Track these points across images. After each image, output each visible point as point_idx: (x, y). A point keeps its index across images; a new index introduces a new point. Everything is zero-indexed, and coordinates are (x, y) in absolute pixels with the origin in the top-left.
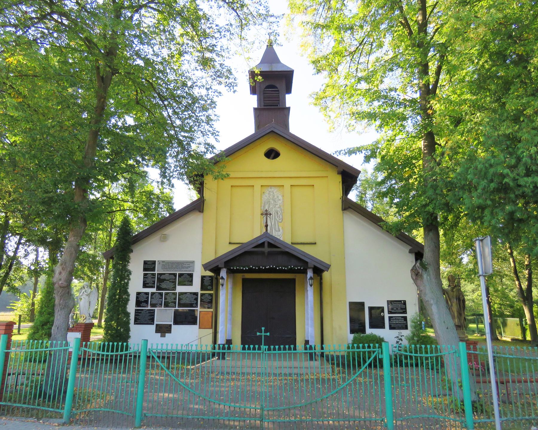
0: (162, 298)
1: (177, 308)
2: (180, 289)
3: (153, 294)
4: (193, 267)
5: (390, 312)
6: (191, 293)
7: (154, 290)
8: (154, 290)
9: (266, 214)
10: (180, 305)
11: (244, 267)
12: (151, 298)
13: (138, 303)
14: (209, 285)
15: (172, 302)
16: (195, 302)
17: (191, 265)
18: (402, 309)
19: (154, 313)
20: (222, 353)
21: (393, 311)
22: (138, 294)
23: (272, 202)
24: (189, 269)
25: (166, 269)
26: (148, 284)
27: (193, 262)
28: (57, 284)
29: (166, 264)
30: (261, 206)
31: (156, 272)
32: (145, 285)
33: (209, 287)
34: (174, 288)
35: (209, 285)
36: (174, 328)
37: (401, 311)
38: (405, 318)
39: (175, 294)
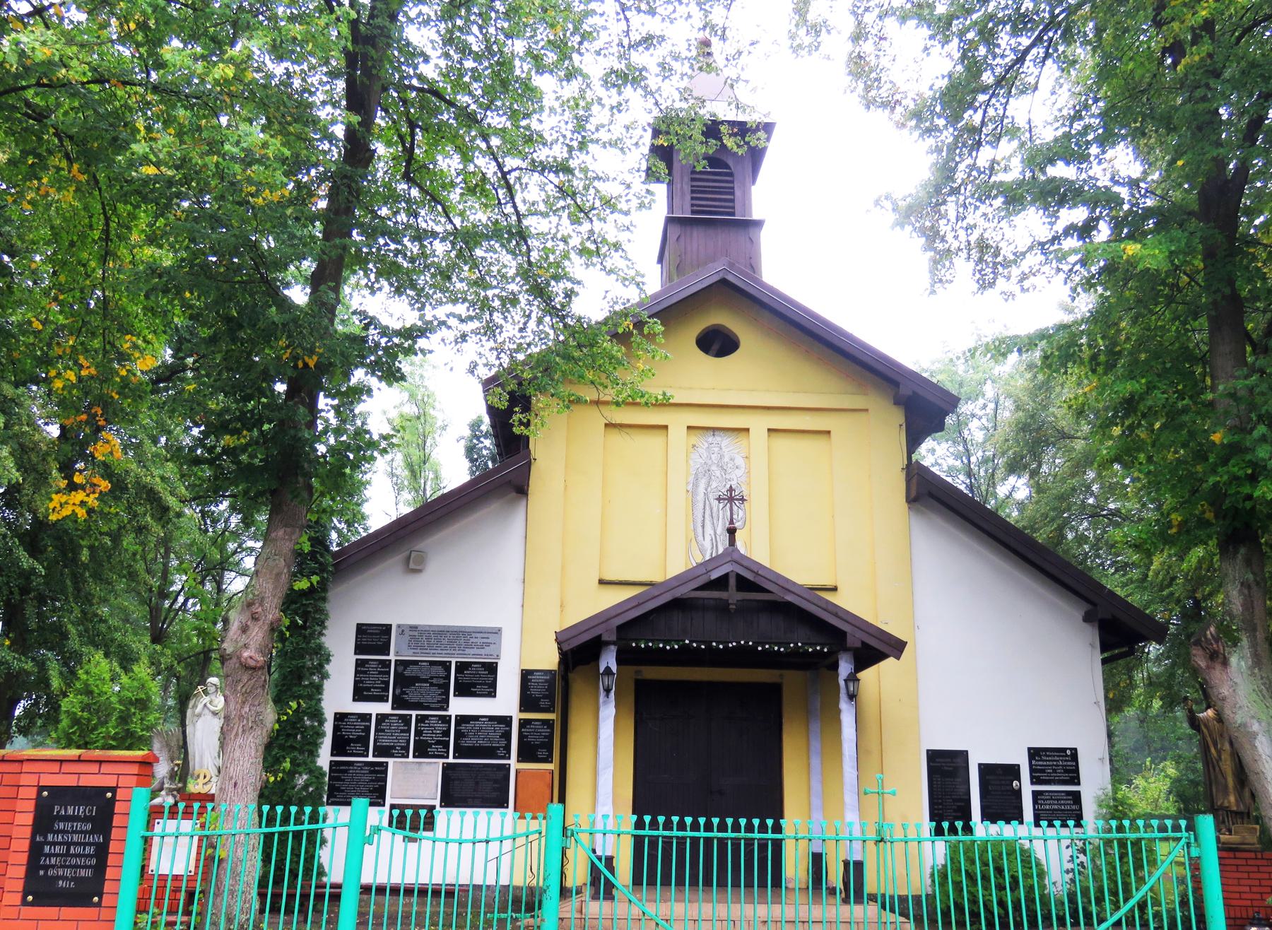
0: (409, 731)
1: (451, 760)
2: (459, 706)
3: (382, 718)
4: (498, 644)
5: (1035, 780)
6: (491, 718)
7: (385, 708)
8: (385, 708)
9: (731, 499)
10: (459, 752)
11: (666, 642)
12: (377, 730)
13: (340, 746)
14: (545, 697)
15: (438, 743)
16: (503, 743)
17: (492, 638)
18: (1066, 771)
19: (385, 772)
20: (692, 838)
21: (1044, 777)
22: (340, 717)
23: (718, 473)
24: (487, 650)
25: (422, 648)
26: (368, 689)
27: (498, 632)
28: (234, 660)
29: (417, 634)
30: (688, 483)
31: (392, 657)
32: (360, 694)
33: (544, 703)
34: (444, 704)
35: (545, 697)
36: (442, 815)
37: (1066, 777)
38: (1076, 797)
39: (446, 720)
